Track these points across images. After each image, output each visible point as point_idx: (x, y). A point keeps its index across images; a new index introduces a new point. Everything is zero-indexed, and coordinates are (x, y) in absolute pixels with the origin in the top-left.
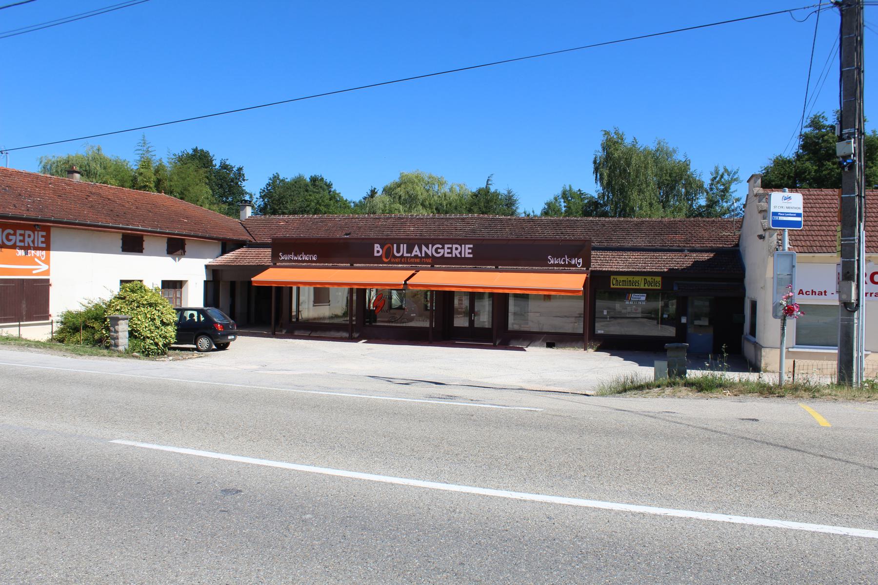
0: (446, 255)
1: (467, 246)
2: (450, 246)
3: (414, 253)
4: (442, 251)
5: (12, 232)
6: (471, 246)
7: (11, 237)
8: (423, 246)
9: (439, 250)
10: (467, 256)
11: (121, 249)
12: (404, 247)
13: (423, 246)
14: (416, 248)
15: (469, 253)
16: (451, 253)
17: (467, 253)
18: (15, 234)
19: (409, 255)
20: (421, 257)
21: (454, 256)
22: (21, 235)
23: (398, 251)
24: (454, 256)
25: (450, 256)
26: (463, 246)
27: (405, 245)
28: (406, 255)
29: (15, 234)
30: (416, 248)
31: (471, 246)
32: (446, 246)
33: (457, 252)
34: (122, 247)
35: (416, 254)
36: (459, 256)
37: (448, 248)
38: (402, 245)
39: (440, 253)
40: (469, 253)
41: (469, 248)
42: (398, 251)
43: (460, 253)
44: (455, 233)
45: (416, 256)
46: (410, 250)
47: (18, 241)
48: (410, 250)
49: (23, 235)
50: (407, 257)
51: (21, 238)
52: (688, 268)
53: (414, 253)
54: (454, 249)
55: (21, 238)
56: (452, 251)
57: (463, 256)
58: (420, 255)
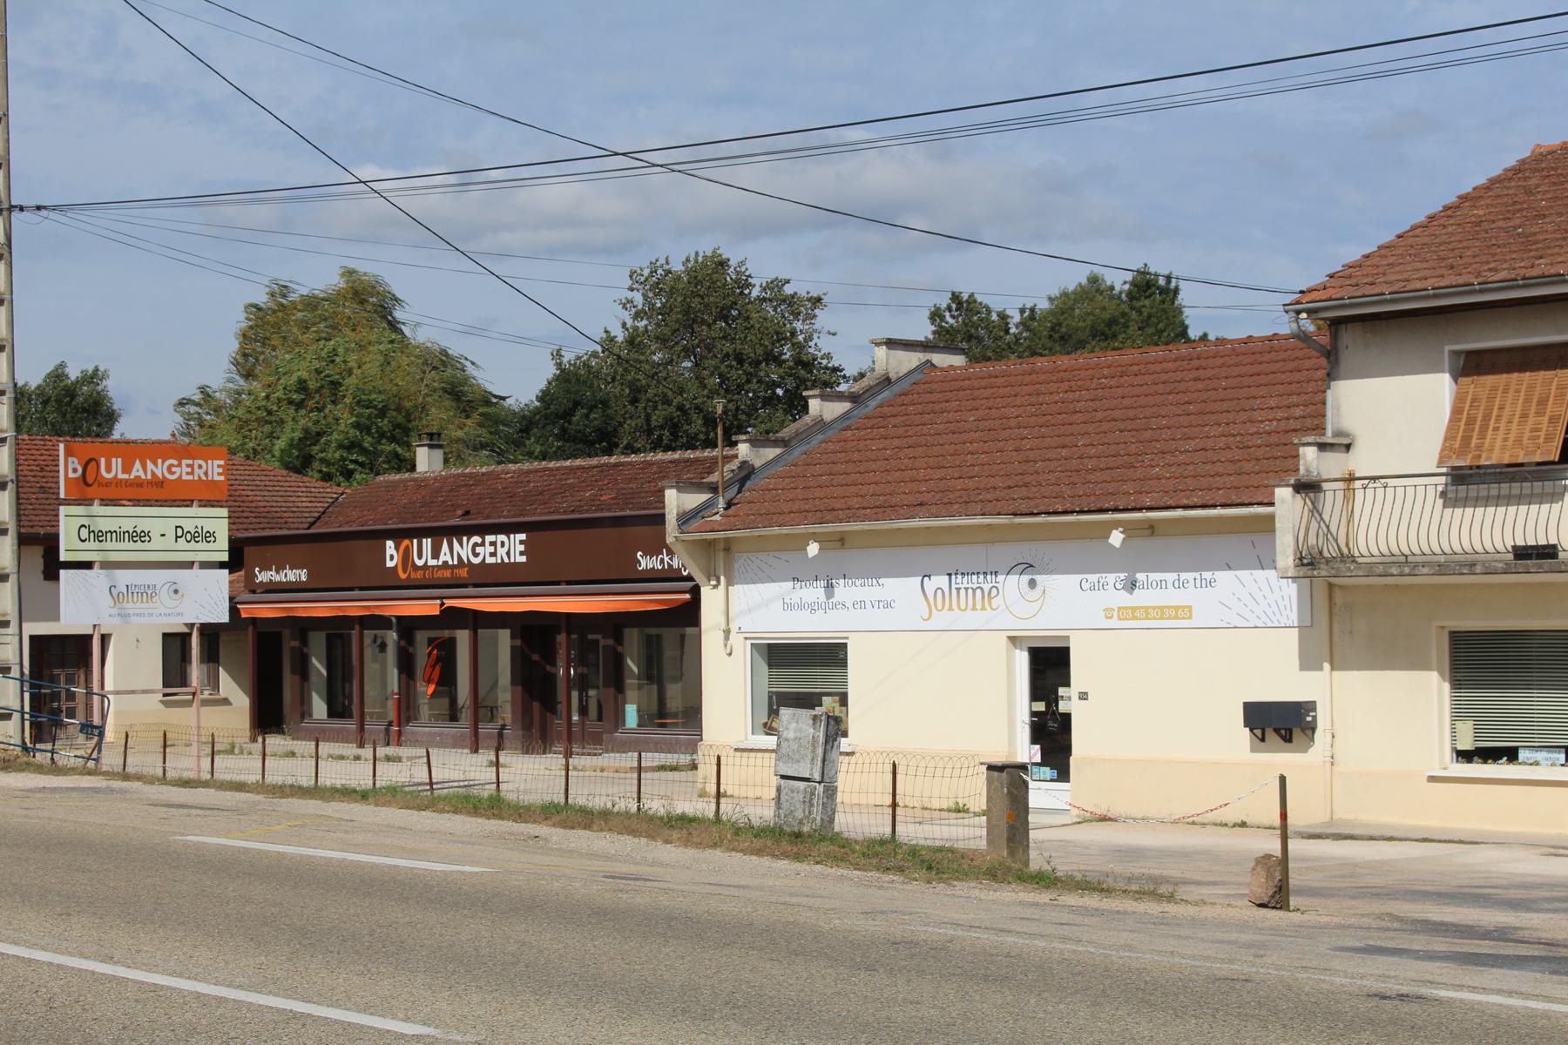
0: (185, 477)
1: (217, 462)
2: (190, 462)
3: (134, 474)
4: (177, 470)
5: (175, 462)
6: (222, 462)
7: (174, 469)
8: (149, 462)
9: (174, 469)
10: (217, 478)
11: (42, 576)
12: (117, 463)
13: (149, 462)
14: (138, 465)
15: (219, 474)
16: (192, 473)
17: (215, 474)
18: (180, 465)
19: (126, 476)
20: (453, 567)
21: (196, 478)
22: (188, 466)
23: (109, 470)
24: (196, 478)
25: (190, 477)
26: (210, 462)
27: (120, 460)
28: (121, 476)
29: (180, 465)
30: (138, 465)
31: (222, 462)
32: (185, 462)
33: (201, 472)
34: (44, 572)
35: (138, 474)
36: (204, 478)
37: (188, 466)
38: (114, 460)
39: (175, 473)
40: (219, 474)
41: (219, 466)
42: (109, 470)
43: (206, 474)
44: (1220, 468)
45: (445, 563)
46: (127, 468)
47: (184, 473)
48: (127, 468)
49: (191, 466)
50: (433, 567)
51: (189, 470)
52: (1515, 372)
53: (134, 474)
54: (196, 467)
55: (189, 470)
56: (193, 469)
57: (210, 478)
58: (143, 477)
